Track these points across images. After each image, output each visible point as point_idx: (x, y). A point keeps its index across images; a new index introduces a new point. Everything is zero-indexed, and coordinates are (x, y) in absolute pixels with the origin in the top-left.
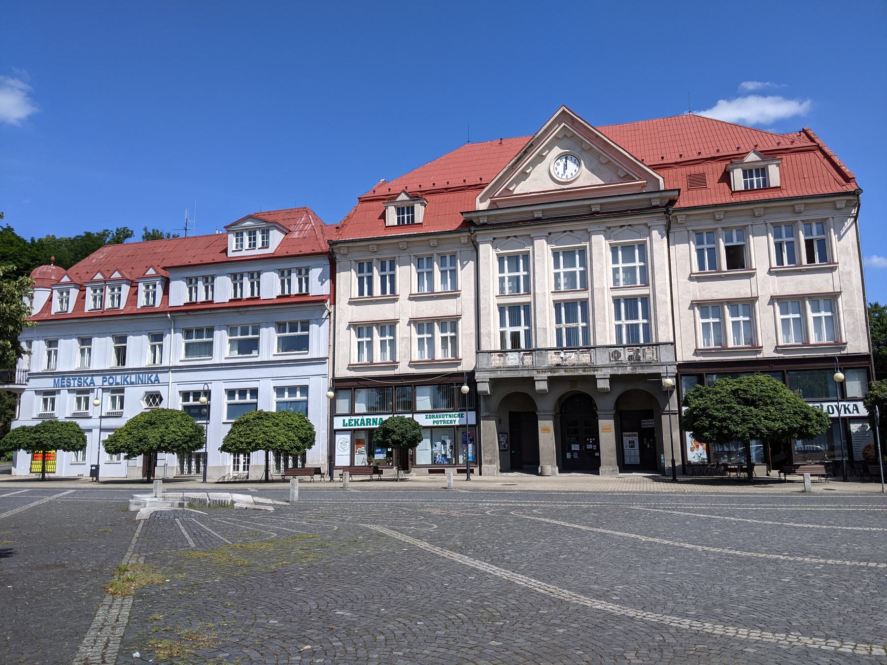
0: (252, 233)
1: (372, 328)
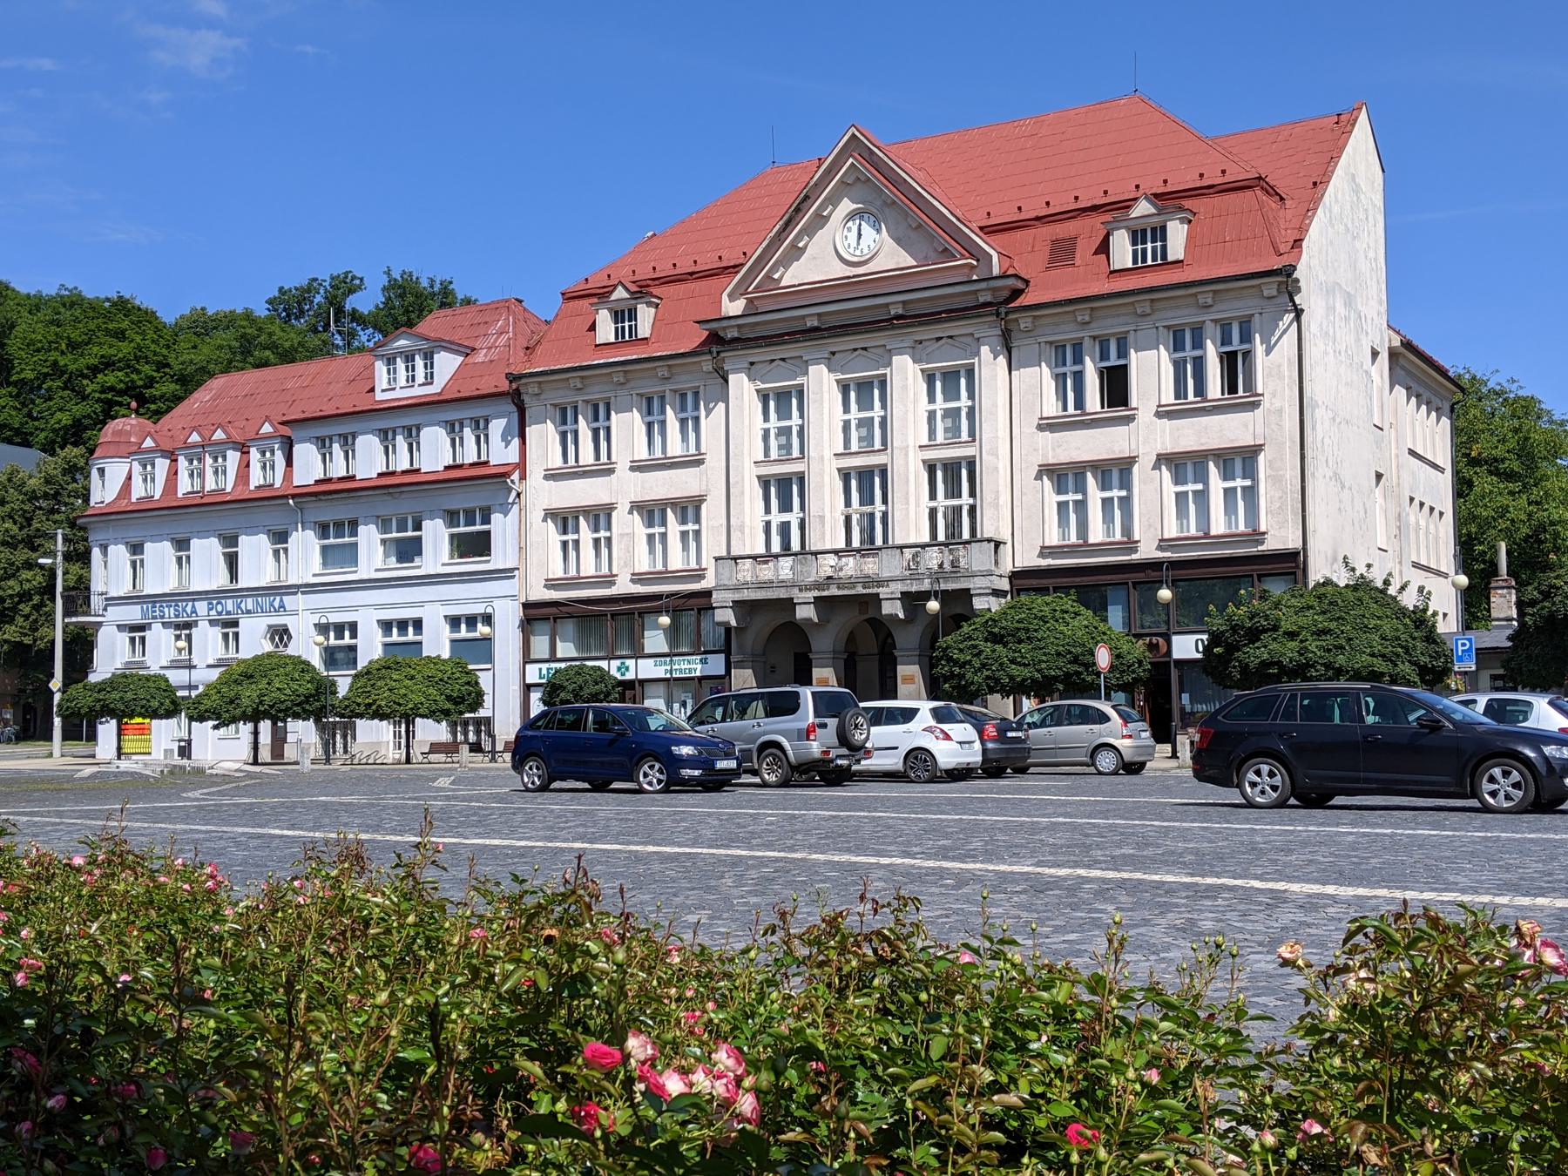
0: (409, 359)
1: (1083, 475)
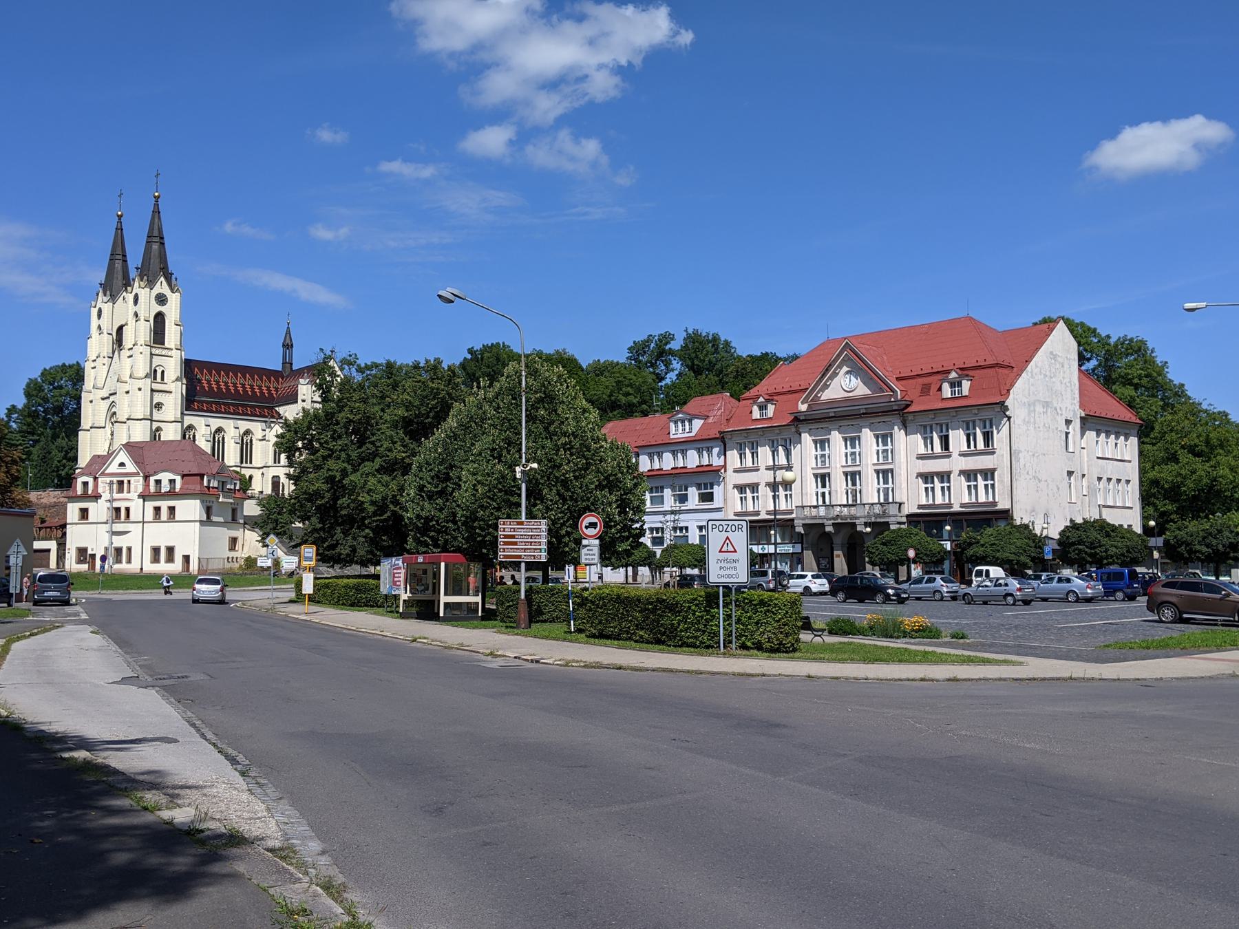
0: (683, 422)
